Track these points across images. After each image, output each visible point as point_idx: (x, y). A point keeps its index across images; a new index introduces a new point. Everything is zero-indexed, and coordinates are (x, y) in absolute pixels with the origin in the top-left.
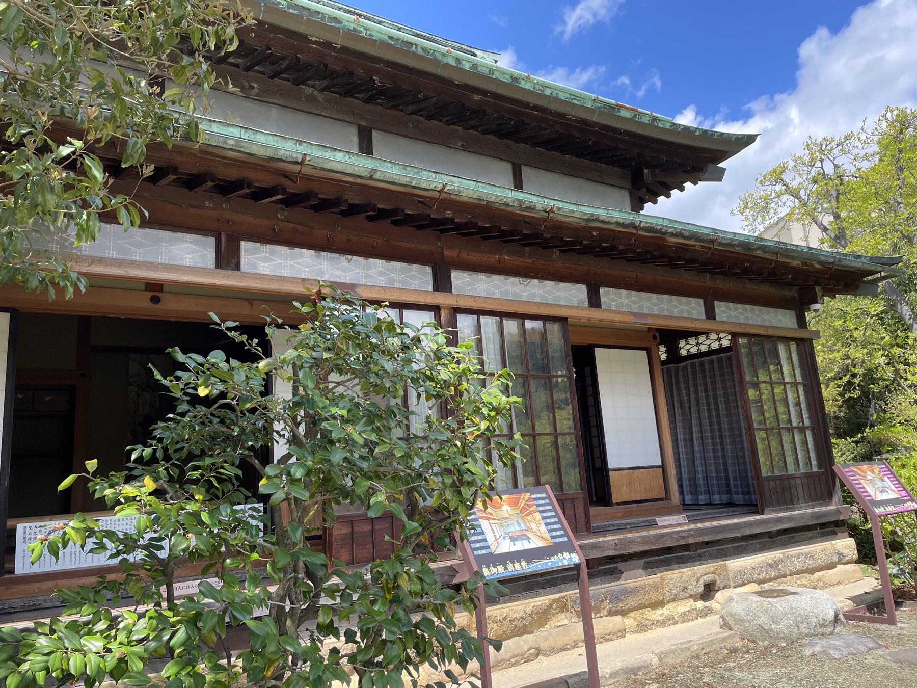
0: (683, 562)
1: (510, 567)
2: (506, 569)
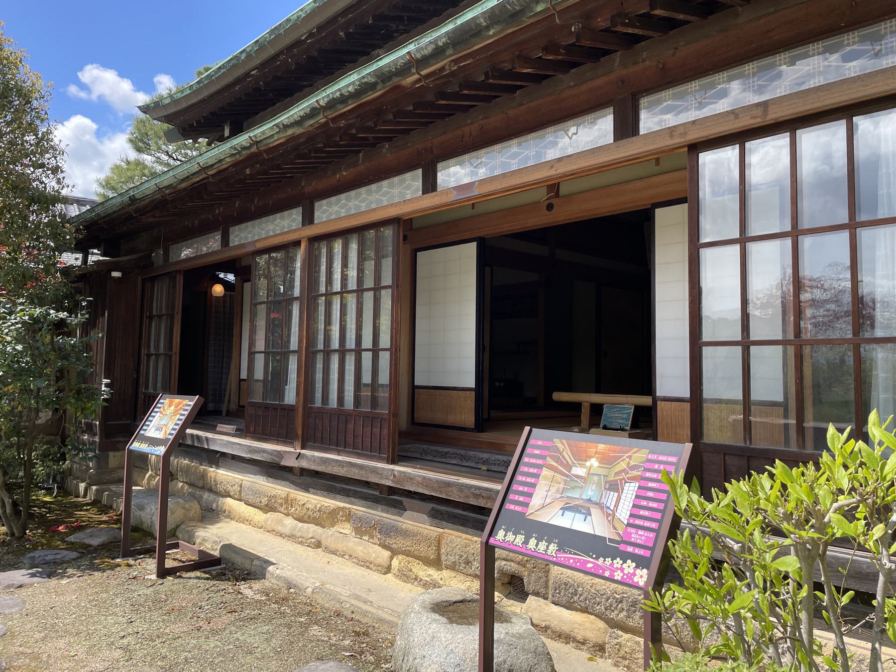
0: (463, 525)
1: (532, 542)
2: (526, 542)
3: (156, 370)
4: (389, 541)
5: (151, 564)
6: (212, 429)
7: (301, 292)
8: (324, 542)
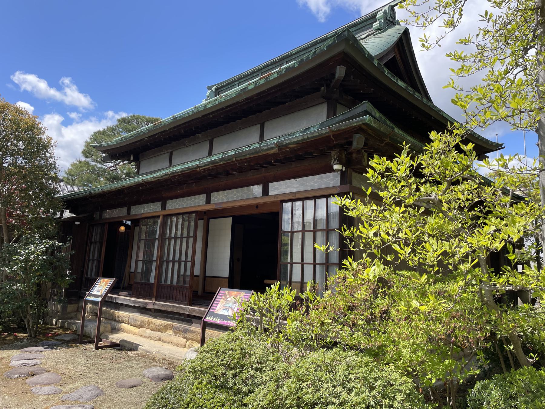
3: (92, 267)
4: (186, 335)
5: (92, 347)
6: (118, 294)
7: (159, 236)
8: (162, 339)
